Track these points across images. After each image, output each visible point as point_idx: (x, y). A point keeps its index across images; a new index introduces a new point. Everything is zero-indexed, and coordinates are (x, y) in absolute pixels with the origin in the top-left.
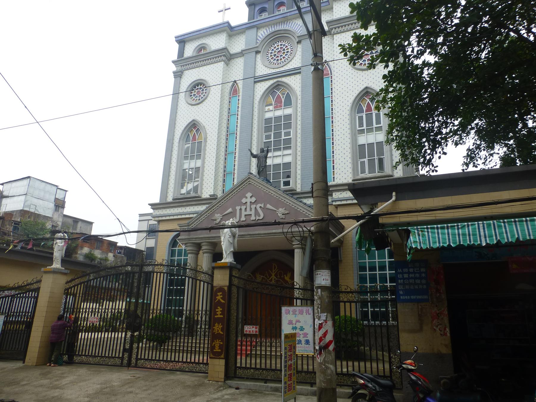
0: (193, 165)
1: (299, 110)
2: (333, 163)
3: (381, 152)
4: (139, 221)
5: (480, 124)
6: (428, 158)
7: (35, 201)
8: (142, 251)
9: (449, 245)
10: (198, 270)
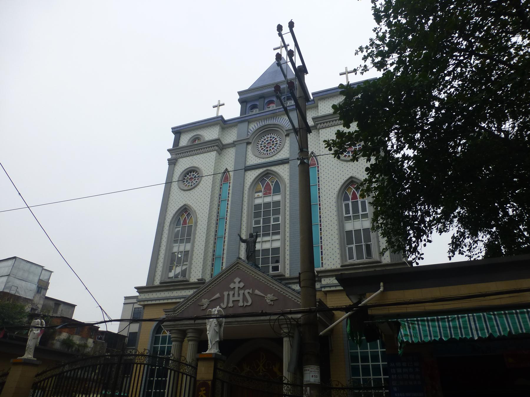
0: (182, 249)
1: (288, 197)
2: (322, 249)
3: (368, 239)
4: (124, 304)
5: (462, 212)
6: (413, 245)
7: (17, 282)
8: (124, 337)
9: (441, 339)
10: (181, 361)
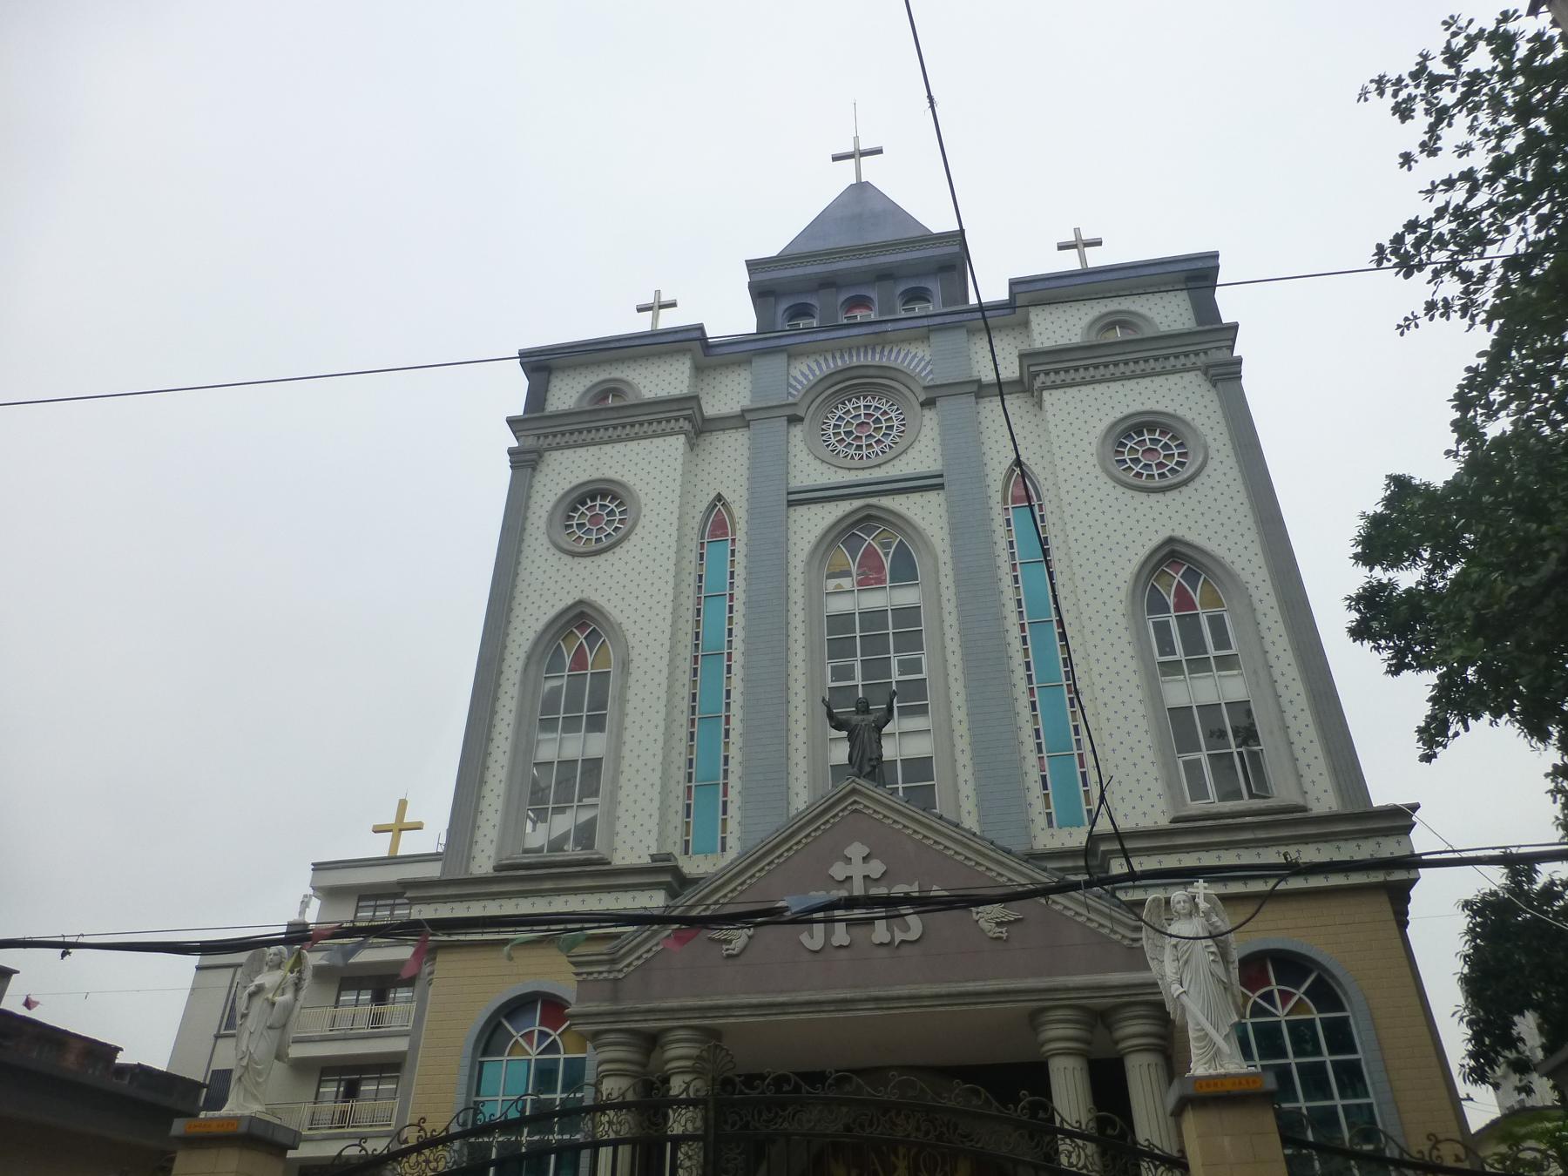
4: (198, 968)
